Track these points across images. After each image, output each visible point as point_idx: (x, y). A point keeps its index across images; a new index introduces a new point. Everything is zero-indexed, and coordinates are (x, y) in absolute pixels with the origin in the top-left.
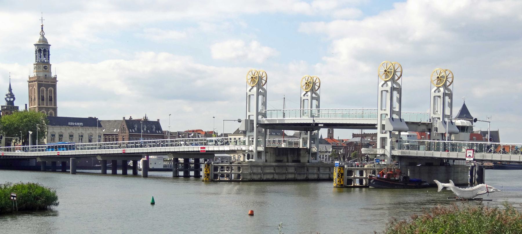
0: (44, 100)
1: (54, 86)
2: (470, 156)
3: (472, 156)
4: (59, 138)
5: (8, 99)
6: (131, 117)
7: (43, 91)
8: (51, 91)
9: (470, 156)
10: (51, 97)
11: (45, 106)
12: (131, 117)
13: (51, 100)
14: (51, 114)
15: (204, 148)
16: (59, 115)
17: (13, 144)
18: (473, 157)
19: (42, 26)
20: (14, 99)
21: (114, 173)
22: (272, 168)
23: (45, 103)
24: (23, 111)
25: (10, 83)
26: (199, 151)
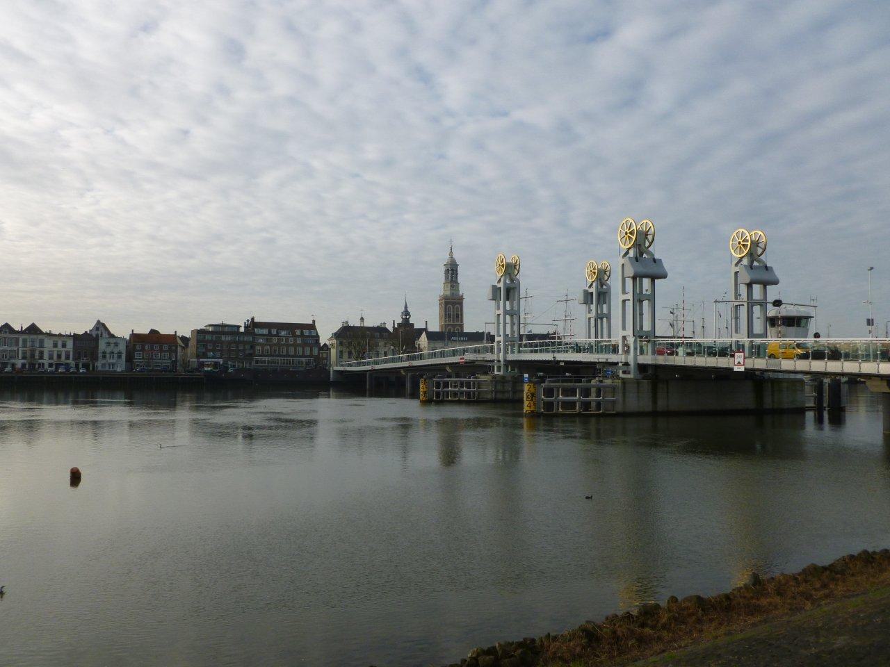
1: (461, 304)
2: (739, 363)
3: (742, 363)
9: (739, 363)
13: (458, 317)
14: (450, 330)
15: (461, 359)
18: (744, 365)
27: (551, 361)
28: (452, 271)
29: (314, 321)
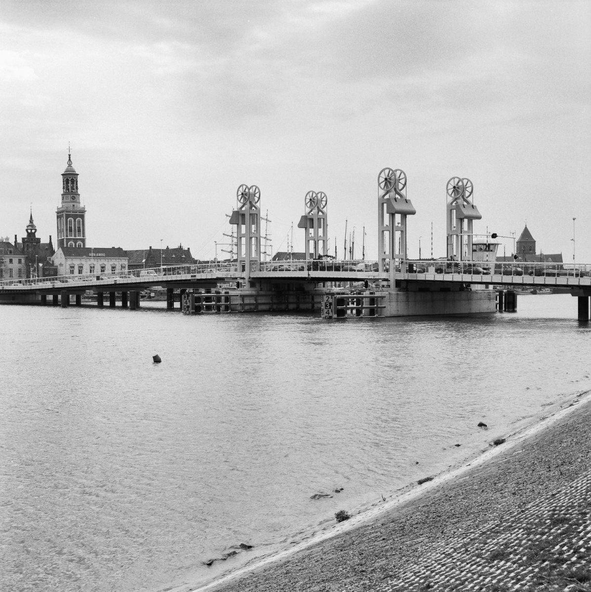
0: (80, 232)
1: (82, 217)
4: (79, 270)
5: (29, 231)
6: (168, 247)
7: (70, 221)
8: (79, 222)
10: (79, 228)
11: (73, 237)
12: (168, 247)
13: (79, 231)
15: (195, 276)
16: (87, 246)
17: (31, 277)
19: (70, 155)
20: (36, 230)
21: (113, 306)
22: (253, 298)
23: (81, 234)
24: (20, 241)
25: (31, 215)
26: (190, 280)
27: (305, 278)
28: (70, 180)
29: (189, 249)
